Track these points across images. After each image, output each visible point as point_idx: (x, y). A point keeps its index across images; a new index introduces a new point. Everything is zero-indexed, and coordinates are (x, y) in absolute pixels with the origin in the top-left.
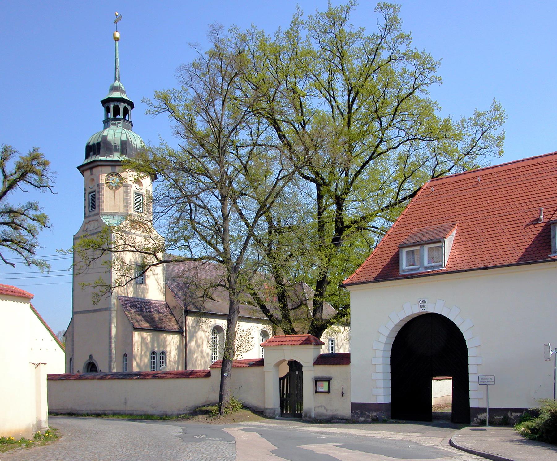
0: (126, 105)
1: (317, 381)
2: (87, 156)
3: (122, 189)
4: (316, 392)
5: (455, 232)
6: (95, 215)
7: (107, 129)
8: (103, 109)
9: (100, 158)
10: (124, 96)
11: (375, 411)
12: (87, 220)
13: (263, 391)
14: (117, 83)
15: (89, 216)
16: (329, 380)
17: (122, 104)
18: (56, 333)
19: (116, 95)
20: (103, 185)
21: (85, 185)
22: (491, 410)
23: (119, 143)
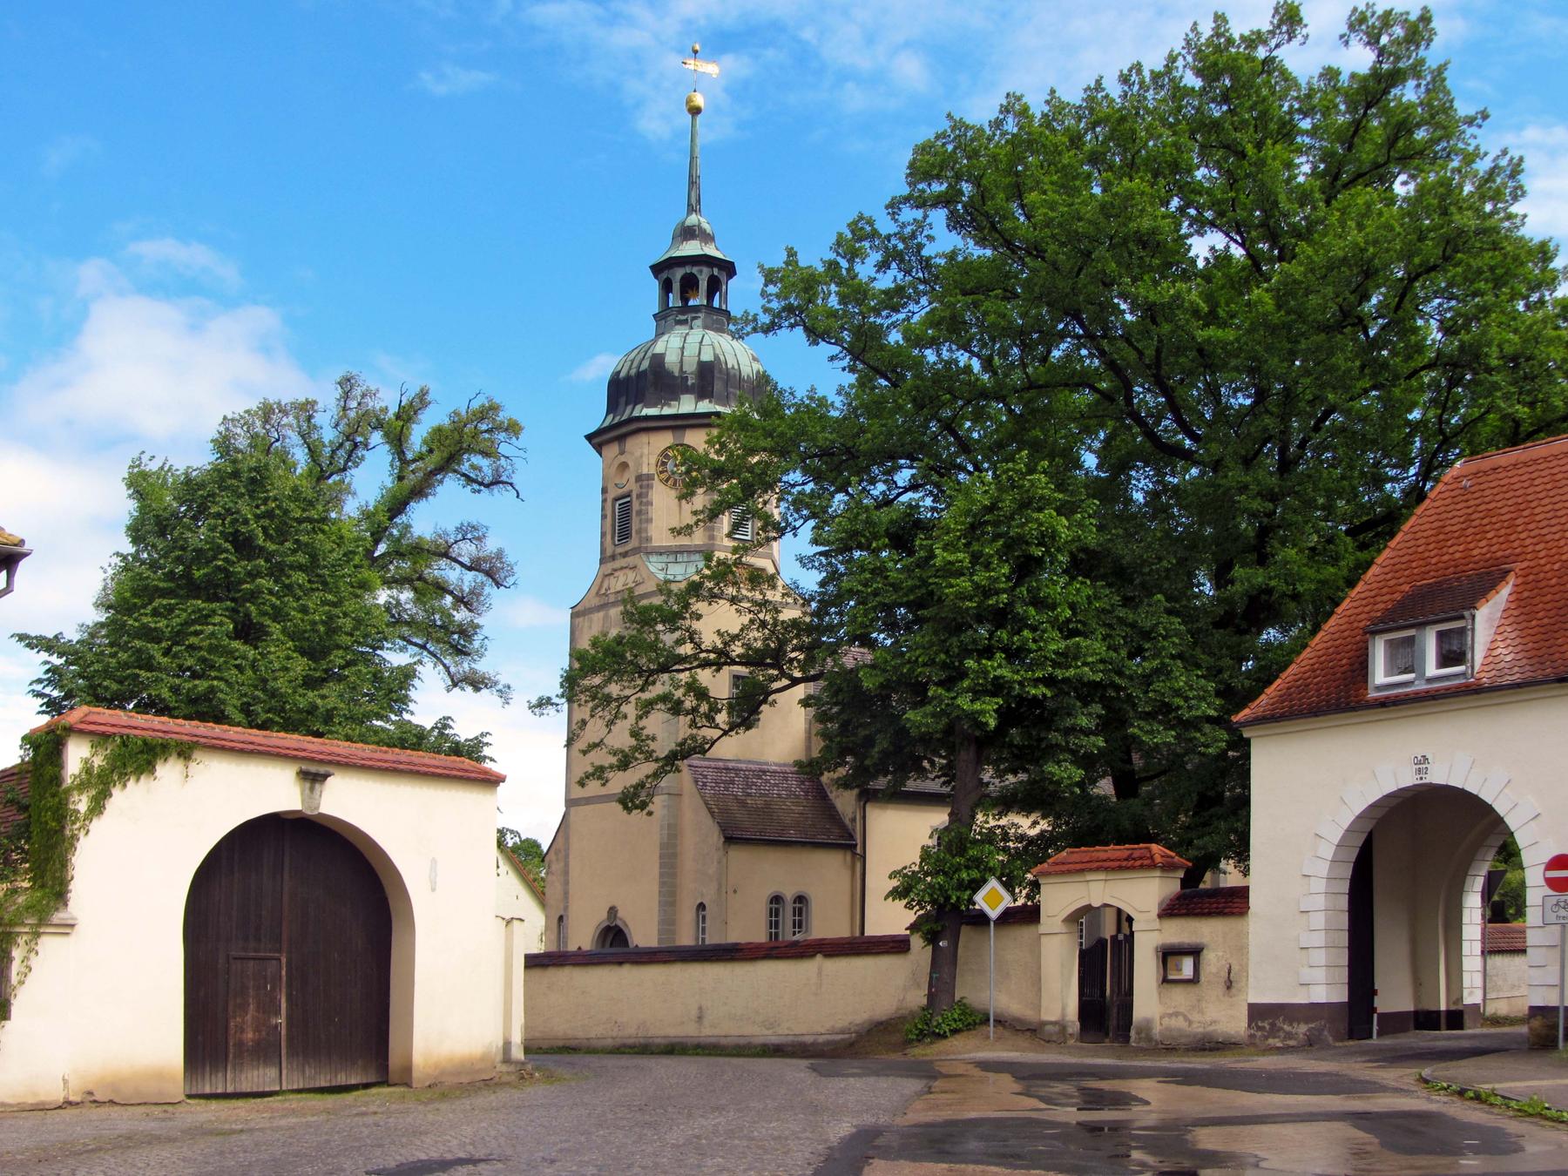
2: (612, 407)
10: (710, 250)
12: (610, 566)
15: (613, 557)
16: (1195, 952)
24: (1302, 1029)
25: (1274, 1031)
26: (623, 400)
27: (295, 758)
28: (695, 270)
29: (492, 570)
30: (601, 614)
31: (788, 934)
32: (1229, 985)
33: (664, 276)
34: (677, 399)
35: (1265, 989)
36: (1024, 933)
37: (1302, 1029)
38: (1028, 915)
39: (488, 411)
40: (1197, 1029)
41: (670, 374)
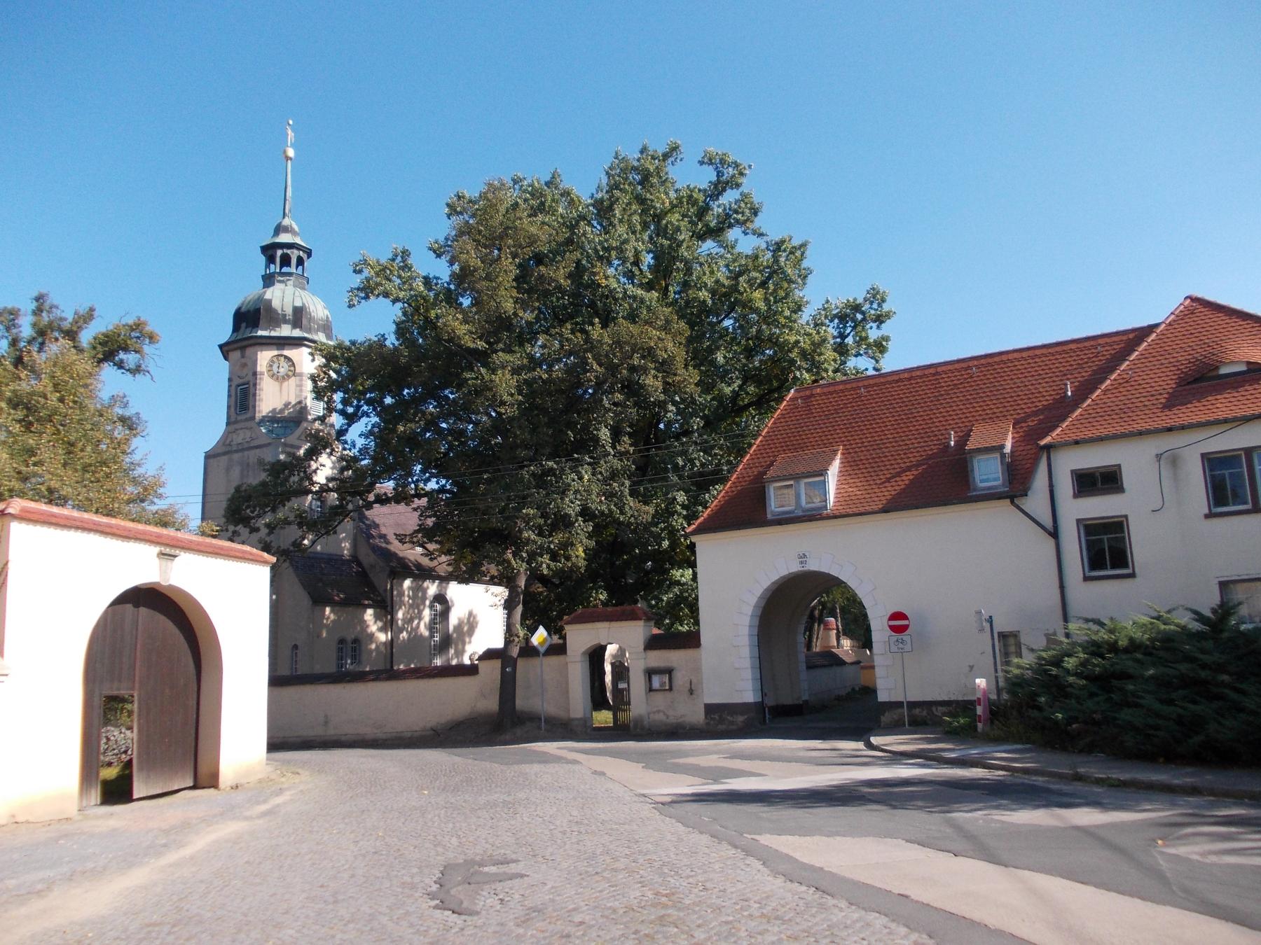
0: (301, 253)
1: (650, 673)
2: (236, 328)
3: (293, 381)
4: (651, 690)
5: (839, 456)
6: (246, 420)
7: (271, 289)
8: (263, 258)
9: (260, 333)
10: (298, 241)
11: (742, 714)
12: (232, 427)
13: (566, 692)
14: (286, 222)
15: (236, 422)
16: (669, 671)
17: (296, 252)
18: (331, 668)
19: (284, 238)
20: (262, 374)
21: (231, 372)
22: (912, 705)
23: (289, 311)
24: (740, 719)
25: (721, 721)
26: (244, 325)
27: (158, 543)
28: (289, 252)
29: (129, 424)
30: (226, 458)
31: (349, 665)
32: (691, 692)
33: (270, 252)
34: (279, 326)
35: (715, 694)
36: (554, 660)
37: (740, 719)
38: (558, 650)
39: (138, 326)
40: (672, 720)
41: (275, 311)
